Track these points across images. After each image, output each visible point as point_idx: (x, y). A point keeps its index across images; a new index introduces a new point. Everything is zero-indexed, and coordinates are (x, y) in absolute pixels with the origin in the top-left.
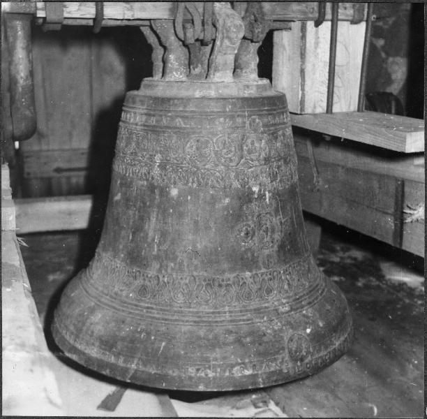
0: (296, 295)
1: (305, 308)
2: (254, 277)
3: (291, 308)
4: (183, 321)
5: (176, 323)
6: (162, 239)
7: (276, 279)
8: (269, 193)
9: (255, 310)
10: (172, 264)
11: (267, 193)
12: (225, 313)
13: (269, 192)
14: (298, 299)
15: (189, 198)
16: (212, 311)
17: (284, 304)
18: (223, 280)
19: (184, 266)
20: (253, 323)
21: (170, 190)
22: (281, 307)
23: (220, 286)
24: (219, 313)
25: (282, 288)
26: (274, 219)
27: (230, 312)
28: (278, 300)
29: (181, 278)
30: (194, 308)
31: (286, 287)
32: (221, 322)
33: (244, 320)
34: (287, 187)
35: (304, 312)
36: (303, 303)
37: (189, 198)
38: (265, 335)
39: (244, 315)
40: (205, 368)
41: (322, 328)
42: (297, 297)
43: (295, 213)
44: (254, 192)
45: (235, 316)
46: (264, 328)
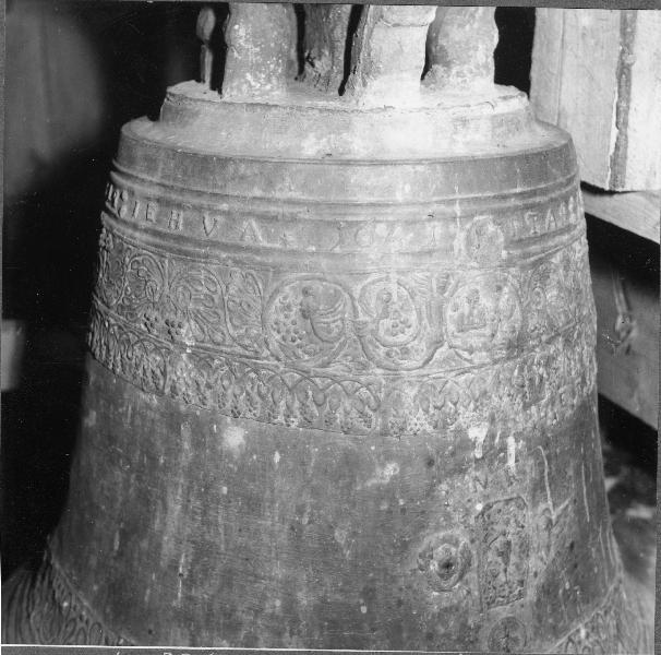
8: (517, 441)
11: (511, 441)
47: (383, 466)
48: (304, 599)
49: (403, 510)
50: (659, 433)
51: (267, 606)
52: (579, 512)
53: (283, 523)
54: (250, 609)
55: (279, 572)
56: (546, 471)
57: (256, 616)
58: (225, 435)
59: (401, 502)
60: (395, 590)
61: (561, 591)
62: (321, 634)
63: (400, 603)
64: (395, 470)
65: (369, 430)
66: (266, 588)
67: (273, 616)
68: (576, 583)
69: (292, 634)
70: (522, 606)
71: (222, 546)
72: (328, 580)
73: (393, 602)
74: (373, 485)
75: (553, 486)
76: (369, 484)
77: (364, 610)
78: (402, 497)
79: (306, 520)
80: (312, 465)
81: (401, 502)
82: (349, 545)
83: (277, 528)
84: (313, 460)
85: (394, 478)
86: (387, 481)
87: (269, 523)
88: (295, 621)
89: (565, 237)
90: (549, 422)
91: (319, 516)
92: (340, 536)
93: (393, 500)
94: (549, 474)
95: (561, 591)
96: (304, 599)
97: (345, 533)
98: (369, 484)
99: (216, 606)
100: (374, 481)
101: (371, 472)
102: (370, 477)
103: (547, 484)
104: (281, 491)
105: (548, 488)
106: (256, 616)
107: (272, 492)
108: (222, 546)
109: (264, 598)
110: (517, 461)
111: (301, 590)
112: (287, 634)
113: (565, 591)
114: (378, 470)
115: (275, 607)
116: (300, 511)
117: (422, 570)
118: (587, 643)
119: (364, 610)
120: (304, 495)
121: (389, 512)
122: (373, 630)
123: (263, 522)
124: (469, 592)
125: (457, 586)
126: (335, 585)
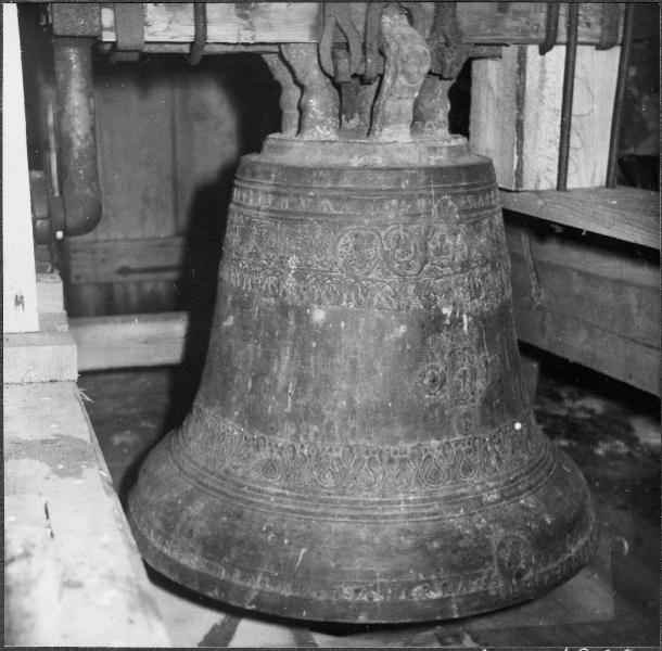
0: (509, 475)
9: (447, 499)
11: (464, 316)
12: (400, 502)
13: (468, 315)
16: (377, 499)
22: (485, 494)
24: (389, 503)
25: (488, 464)
31: (493, 462)
35: (522, 502)
36: (520, 487)
39: (428, 507)
41: (549, 526)
109: (336, 401)
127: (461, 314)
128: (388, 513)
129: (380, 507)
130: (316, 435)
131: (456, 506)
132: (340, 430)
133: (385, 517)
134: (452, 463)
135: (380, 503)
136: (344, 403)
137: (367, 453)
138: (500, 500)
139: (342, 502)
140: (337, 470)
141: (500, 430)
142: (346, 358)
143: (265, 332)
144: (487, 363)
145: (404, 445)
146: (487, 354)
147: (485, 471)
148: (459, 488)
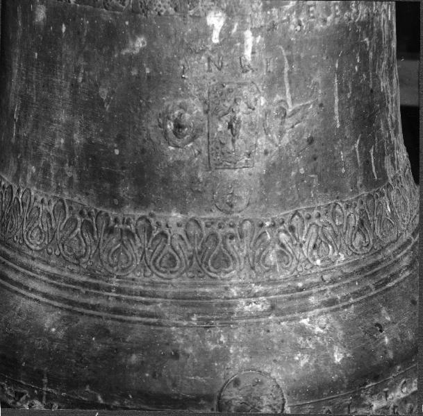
0: (296, 279)
1: (311, 314)
2: (187, 226)
3: (273, 308)
4: (26, 288)
5: (15, 288)
6: (22, 113)
7: (247, 239)
8: (255, 35)
9: (176, 297)
10: (34, 169)
11: (248, 34)
12: (109, 289)
13: (255, 32)
14: (301, 290)
15: (64, 29)
16: (84, 279)
17: (255, 296)
18: (116, 220)
19: (50, 174)
20: (160, 325)
21: (34, 8)
22: (242, 301)
23: (110, 231)
24: (97, 287)
25: (261, 259)
26: (262, 101)
27: (119, 290)
28: (242, 285)
29: (42, 201)
30: (53, 266)
31: (272, 258)
32: (94, 307)
33: (142, 315)
34: (319, 26)
35: (305, 322)
36: (312, 300)
37: (64, 29)
38: (176, 356)
39: (147, 303)
40: (33, 397)
41: (338, 366)
42: (300, 285)
43: (341, 92)
44: (293, 41)
45: (128, 301)
46: (181, 341)
47: (134, 39)
48: (78, 139)
49: (149, 77)
50: (421, 111)
51: (56, 143)
52: (326, 114)
53: (67, 81)
54: (46, 144)
55: (63, 117)
56: (286, 70)
57: (50, 150)
58: (36, 13)
59: (148, 71)
60: (140, 140)
61: (293, 173)
62: (87, 166)
63: (143, 151)
64: (143, 43)
65: (124, 7)
66: (56, 130)
67: (59, 151)
68: (314, 171)
69: (70, 164)
70: (250, 174)
71: (35, 98)
72: (93, 127)
73: (138, 149)
74: (126, 54)
75: (293, 84)
76: (123, 53)
77: (117, 152)
78: (148, 66)
79: (80, 79)
80: (85, 35)
81: (148, 71)
82: (108, 100)
83: (63, 85)
84: (86, 31)
85: (142, 50)
86: (137, 51)
87: (59, 80)
88: (72, 155)
89: (167, 281)
90: (292, 27)
91: (89, 76)
92: (104, 92)
93: (141, 68)
94: (289, 73)
95: (293, 173)
96: (78, 139)
97: (106, 92)
98: (123, 53)
99: (29, 142)
100: (127, 51)
101: (124, 45)
102: (124, 48)
103: (286, 80)
104: (66, 55)
105: (287, 85)
106: (50, 150)
107: (61, 56)
108: (35, 98)
109: (54, 136)
110: (253, 53)
111: (76, 133)
112: (67, 165)
113: (298, 174)
114: (131, 43)
115: (60, 143)
116: (77, 71)
117: (161, 127)
118: (316, 221)
119: (117, 152)
120: (80, 58)
121: (138, 77)
122: (123, 168)
123: (56, 80)
124: (200, 152)
125: (189, 145)
126: (96, 130)
127: (242, 28)
128: (92, 301)
129: (83, 291)
130: (33, 178)
131: (190, 311)
132: (56, 176)
133: (86, 306)
134: (198, 248)
135: (84, 284)
136: (62, 141)
137: (81, 213)
138: (266, 314)
139: (43, 273)
140: (46, 229)
141: (296, 213)
142: (67, 78)
143: (230, 41)
144: (283, 110)
145: (132, 213)
146: (288, 97)
147: (253, 268)
148: (203, 285)
